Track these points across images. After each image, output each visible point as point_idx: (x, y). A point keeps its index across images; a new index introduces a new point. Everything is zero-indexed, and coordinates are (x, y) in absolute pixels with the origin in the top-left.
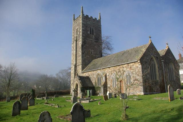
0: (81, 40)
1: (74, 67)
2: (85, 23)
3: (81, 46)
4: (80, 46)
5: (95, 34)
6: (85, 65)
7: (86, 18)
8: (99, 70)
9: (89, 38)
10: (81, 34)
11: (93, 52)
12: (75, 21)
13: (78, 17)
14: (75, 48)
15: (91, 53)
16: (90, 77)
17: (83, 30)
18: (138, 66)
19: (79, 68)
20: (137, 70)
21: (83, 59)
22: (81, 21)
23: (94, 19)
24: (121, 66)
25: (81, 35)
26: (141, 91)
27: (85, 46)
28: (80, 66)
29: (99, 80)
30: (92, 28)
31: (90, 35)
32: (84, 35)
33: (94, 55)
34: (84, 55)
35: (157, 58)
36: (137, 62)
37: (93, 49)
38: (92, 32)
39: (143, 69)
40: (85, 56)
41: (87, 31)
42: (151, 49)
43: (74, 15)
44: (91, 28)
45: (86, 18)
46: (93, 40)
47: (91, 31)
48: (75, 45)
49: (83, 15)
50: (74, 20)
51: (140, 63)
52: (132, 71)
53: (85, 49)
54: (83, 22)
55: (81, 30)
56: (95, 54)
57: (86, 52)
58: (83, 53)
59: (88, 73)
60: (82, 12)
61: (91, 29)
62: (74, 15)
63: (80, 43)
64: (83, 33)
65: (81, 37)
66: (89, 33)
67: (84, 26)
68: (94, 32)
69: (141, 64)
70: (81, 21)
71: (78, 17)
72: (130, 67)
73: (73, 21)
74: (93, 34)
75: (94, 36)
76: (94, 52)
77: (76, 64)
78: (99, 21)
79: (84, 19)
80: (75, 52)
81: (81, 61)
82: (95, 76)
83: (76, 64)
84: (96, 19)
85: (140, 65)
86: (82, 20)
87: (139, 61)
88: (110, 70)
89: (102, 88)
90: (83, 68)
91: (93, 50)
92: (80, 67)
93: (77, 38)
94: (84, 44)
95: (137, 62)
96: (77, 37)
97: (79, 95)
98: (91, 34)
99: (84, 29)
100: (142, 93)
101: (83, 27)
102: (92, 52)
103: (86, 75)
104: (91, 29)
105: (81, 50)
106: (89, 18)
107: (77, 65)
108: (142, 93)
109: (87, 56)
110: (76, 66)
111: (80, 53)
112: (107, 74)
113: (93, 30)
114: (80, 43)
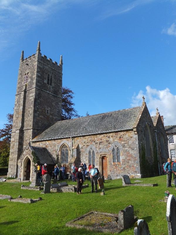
0: (34, 91)
1: (18, 131)
2: (41, 67)
3: (33, 100)
4: (31, 100)
5: (53, 84)
6: (37, 131)
7: (43, 60)
8: (64, 140)
9: (45, 89)
10: (35, 81)
11: (49, 112)
12: (24, 61)
13: (30, 57)
14: (22, 102)
15: (46, 112)
16: (49, 149)
17: (38, 76)
18: (134, 137)
19: (28, 134)
20: (130, 142)
21: (35, 121)
22: (36, 64)
23: (53, 63)
24: (105, 135)
25: (35, 83)
26: (136, 172)
27: (39, 101)
28: (29, 131)
29: (64, 155)
30: (50, 75)
31: (47, 85)
32: (38, 84)
33: (51, 116)
34: (37, 115)
35: (151, 126)
36: (132, 130)
37: (50, 107)
38: (50, 81)
39: (140, 140)
40: (38, 116)
41: (43, 80)
42: (146, 114)
43: (23, 52)
44: (49, 75)
45: (43, 60)
46: (50, 93)
47: (48, 80)
48: (22, 97)
49: (40, 54)
50: (23, 59)
51: (136, 133)
52: (123, 142)
53: (39, 106)
54: (39, 65)
55: (35, 76)
56: (52, 115)
57: (40, 110)
58: (35, 111)
59: (44, 142)
60: (39, 50)
61: (48, 77)
62: (23, 52)
63: (31, 95)
64: (38, 81)
65: (34, 86)
66: (46, 81)
67: (39, 70)
68: (53, 81)
69: (138, 133)
70: (36, 63)
71: (30, 57)
72: (120, 138)
73: (21, 61)
74: (51, 85)
75: (53, 88)
76: (51, 111)
77: (23, 126)
78: (60, 68)
79: (41, 60)
80: (21, 107)
81: (31, 123)
82: (57, 148)
83: (23, 126)
84: (56, 63)
85: (136, 134)
86: (38, 61)
87: (135, 130)
88: (85, 140)
89: (159, 157)
90: (34, 135)
91: (49, 108)
92: (30, 132)
93: (26, 87)
94: (37, 98)
95: (132, 130)
96: (26, 85)
97: (32, 178)
98: (48, 83)
99: (40, 75)
100: (139, 175)
101: (38, 72)
102: (48, 110)
103: (39, 145)
104: (48, 77)
105: (32, 106)
106: (48, 60)
107: (24, 129)
108: (138, 175)
109: (41, 116)
110: (22, 131)
111: (30, 110)
112: (80, 146)
113: (51, 78)
114: (32, 96)
